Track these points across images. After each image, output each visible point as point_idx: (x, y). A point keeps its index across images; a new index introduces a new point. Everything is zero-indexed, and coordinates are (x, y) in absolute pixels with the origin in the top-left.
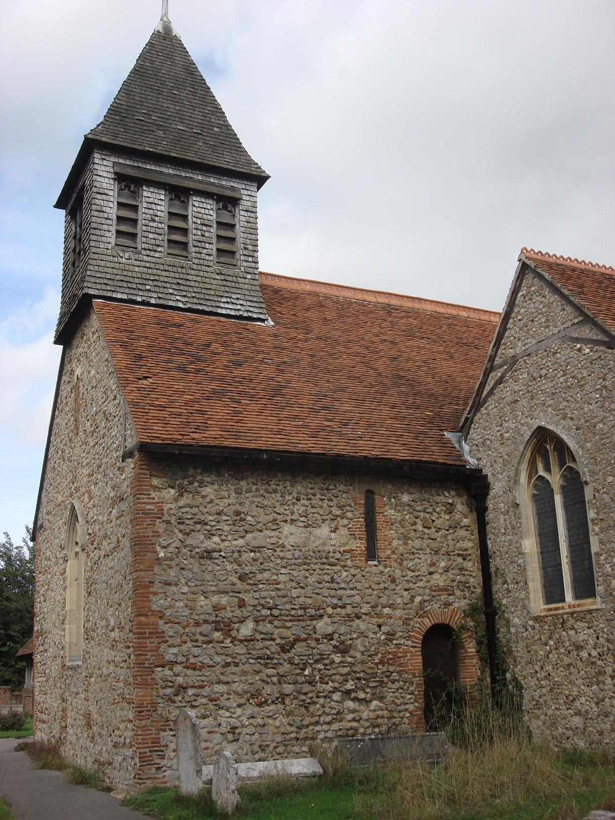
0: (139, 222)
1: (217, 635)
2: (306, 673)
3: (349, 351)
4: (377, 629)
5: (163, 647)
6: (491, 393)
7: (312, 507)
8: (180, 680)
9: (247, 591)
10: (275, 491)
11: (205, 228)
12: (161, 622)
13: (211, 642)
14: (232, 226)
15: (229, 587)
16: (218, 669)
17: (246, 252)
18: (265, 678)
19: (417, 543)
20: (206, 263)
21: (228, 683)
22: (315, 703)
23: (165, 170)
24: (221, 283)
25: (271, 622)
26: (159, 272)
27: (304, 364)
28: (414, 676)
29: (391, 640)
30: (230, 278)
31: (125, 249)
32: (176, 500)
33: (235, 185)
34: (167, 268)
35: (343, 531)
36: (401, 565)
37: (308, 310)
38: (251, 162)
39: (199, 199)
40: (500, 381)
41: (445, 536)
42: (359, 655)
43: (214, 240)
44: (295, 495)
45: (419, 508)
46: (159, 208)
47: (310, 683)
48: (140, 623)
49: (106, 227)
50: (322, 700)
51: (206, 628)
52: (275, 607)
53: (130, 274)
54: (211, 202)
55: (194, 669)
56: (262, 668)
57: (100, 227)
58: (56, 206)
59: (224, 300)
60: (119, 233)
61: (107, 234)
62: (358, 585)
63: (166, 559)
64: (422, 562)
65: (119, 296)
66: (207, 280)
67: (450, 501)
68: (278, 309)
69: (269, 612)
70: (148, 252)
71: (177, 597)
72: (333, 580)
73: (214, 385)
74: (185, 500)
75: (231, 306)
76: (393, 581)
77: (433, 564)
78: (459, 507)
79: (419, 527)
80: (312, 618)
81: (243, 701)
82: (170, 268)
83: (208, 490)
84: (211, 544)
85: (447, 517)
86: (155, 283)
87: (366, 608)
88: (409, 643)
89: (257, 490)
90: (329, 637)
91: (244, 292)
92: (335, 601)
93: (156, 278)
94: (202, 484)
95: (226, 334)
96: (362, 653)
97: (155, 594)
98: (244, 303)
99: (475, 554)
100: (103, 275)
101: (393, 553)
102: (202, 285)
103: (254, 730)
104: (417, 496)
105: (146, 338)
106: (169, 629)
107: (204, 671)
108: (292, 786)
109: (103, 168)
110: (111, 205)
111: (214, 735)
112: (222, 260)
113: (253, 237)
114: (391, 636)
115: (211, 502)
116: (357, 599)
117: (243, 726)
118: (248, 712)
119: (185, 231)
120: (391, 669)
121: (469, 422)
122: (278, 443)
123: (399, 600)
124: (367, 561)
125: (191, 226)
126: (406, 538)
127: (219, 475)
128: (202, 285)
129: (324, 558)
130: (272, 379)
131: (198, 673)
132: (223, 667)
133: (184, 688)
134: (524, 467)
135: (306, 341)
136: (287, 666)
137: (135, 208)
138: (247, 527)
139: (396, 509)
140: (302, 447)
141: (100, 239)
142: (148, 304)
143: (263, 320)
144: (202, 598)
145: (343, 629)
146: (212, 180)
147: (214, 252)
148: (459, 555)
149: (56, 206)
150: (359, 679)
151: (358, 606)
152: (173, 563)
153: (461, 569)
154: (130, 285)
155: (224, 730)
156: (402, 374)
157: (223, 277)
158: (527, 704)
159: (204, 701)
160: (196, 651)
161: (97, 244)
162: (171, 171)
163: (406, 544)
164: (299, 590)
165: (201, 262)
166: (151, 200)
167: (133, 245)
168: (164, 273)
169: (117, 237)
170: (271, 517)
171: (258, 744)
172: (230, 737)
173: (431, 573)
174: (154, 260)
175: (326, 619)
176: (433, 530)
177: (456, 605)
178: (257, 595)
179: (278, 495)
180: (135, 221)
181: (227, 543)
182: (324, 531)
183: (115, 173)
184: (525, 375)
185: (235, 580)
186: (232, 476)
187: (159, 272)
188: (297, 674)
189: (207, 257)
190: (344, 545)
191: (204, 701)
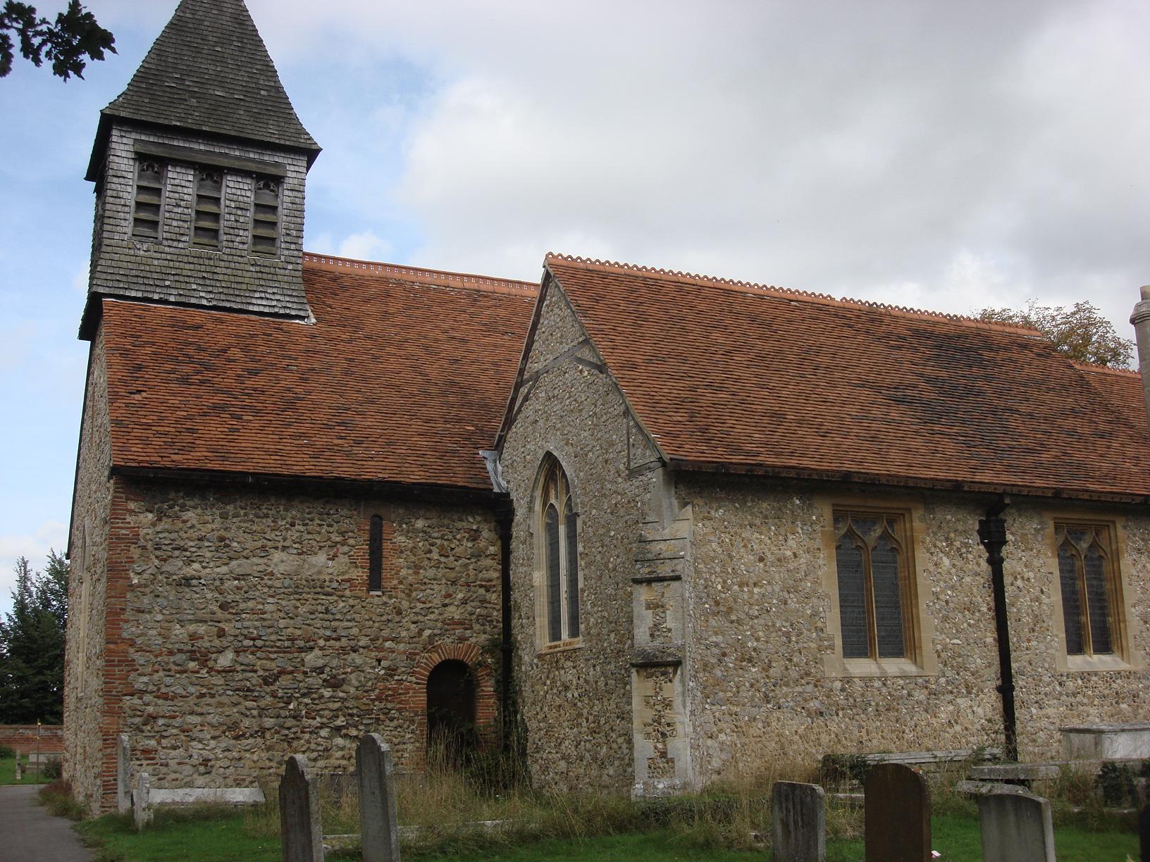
0: (162, 208)
1: (192, 665)
2: (291, 707)
3: (402, 353)
4: (375, 663)
5: (133, 675)
6: (519, 411)
7: (309, 533)
8: (150, 709)
9: (228, 621)
10: (266, 516)
11: (239, 212)
12: (132, 650)
13: (185, 672)
14: (274, 209)
15: (208, 616)
16: (192, 700)
17: (288, 239)
18: (244, 711)
19: (431, 573)
20: (239, 253)
21: (202, 714)
22: (298, 738)
23: (195, 146)
24: (255, 275)
25: (253, 653)
26: (182, 265)
27: (336, 370)
28: (416, 715)
29: (392, 676)
30: (267, 270)
31: (144, 239)
32: (154, 524)
33: (280, 160)
34: (191, 260)
35: (343, 559)
36: (409, 595)
37: (367, 301)
38: (301, 131)
39: (234, 178)
40: (526, 399)
41: (466, 565)
42: (352, 690)
43: (250, 226)
44: (289, 520)
45: (436, 535)
46: (186, 190)
47: (294, 717)
48: (109, 651)
49: (122, 215)
50: (307, 736)
51: (180, 657)
52: (259, 637)
53: (147, 268)
54: (249, 181)
55: (166, 699)
56: (241, 700)
57: (116, 215)
58: (86, 179)
59: (257, 295)
60: (137, 221)
61: (123, 223)
62: (357, 617)
63: (139, 585)
64: (436, 593)
65: (133, 294)
66: (240, 273)
67: (475, 527)
68: (329, 302)
69: (251, 643)
70: (170, 243)
71: (150, 625)
72: (327, 611)
73: (217, 399)
74: (165, 524)
75: (264, 302)
76: (399, 613)
77: (448, 596)
78: (485, 534)
79: (435, 556)
80: (301, 650)
81: (217, 733)
82: (196, 260)
83: (189, 515)
84: (189, 571)
85: (470, 545)
86: (177, 278)
87: (364, 641)
88: (413, 679)
89: (246, 514)
90: (320, 670)
91: (283, 285)
92: (328, 633)
93: (178, 271)
94: (183, 508)
95: (252, 336)
96: (357, 688)
97: (127, 621)
98: (281, 298)
99: (498, 584)
100: (116, 271)
101: (401, 582)
102: (232, 279)
103: (228, 763)
104: (435, 521)
105: (153, 344)
106: (140, 658)
107: (176, 702)
108: (222, 811)
109: (122, 147)
110: (129, 189)
111: (184, 767)
112: (259, 248)
113: (299, 220)
114: (391, 671)
115: (193, 527)
116: (355, 631)
117: (217, 759)
118: (223, 745)
119: (216, 217)
120: (390, 705)
121: (502, 439)
122: (271, 465)
123: (404, 634)
124: (368, 591)
125: (223, 210)
126: (417, 568)
127: (204, 498)
128: (232, 279)
129: (317, 586)
130: (289, 390)
131: (169, 703)
132: (198, 697)
133: (154, 718)
134: (538, 493)
135: (350, 341)
136: (269, 699)
137: (158, 192)
138: (231, 554)
139: (406, 538)
140: (296, 470)
141: (114, 229)
142: (166, 302)
143: (302, 318)
144: (178, 626)
145: (335, 662)
146: (252, 155)
147: (250, 239)
148: (481, 586)
149: (86, 179)
150: (351, 715)
151: (355, 638)
152: (148, 590)
153: (483, 601)
154: (146, 281)
155: (195, 762)
156: (457, 379)
157: (258, 269)
158: (530, 748)
159: (175, 731)
160: (168, 680)
161: (111, 235)
162: (202, 147)
163: (416, 573)
164: (288, 620)
165: (233, 251)
166: (176, 182)
167: (153, 234)
168: (187, 266)
169: (135, 226)
170: (259, 544)
171: (232, 778)
172: (202, 769)
173: (445, 605)
174: (177, 251)
175: (317, 652)
176: (452, 558)
177: (473, 640)
178: (239, 625)
179: (269, 520)
180: (157, 207)
181: (208, 571)
182: (321, 558)
183: (136, 153)
184: (543, 394)
185: (215, 609)
186: (218, 500)
187: (182, 265)
188: (281, 708)
189: (241, 246)
190: (343, 573)
191: (175, 731)
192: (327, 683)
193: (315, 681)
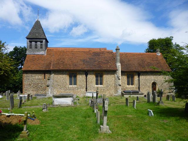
182: (40, 77)
192: (41, 87)
193: (40, 87)
